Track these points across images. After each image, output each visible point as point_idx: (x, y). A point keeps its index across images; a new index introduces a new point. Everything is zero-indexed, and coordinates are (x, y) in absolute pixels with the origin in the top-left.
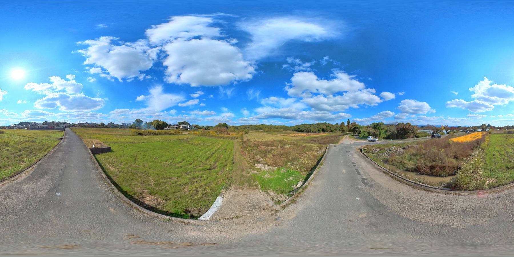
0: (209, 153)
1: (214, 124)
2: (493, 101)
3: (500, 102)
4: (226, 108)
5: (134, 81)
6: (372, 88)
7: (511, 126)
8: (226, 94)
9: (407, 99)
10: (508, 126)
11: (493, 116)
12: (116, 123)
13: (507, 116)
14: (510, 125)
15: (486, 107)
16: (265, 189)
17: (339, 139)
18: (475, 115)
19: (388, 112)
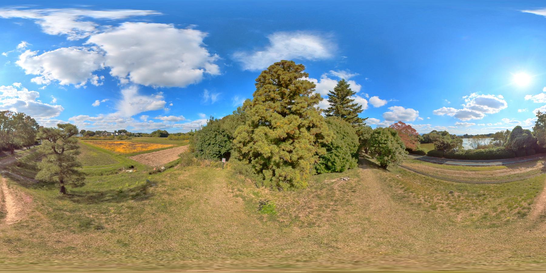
0: (392, 175)
1: (185, 131)
2: (485, 111)
3: (491, 111)
4: (203, 113)
5: (85, 87)
6: (95, 102)
7: (495, 133)
8: (210, 100)
9: (410, 108)
10: (467, 135)
11: (482, 124)
12: (129, 131)
13: (496, 124)
14: (94, 131)
15: (477, 116)
16: (275, 220)
17: (32, 142)
18: (462, 123)
19: (374, 119)
